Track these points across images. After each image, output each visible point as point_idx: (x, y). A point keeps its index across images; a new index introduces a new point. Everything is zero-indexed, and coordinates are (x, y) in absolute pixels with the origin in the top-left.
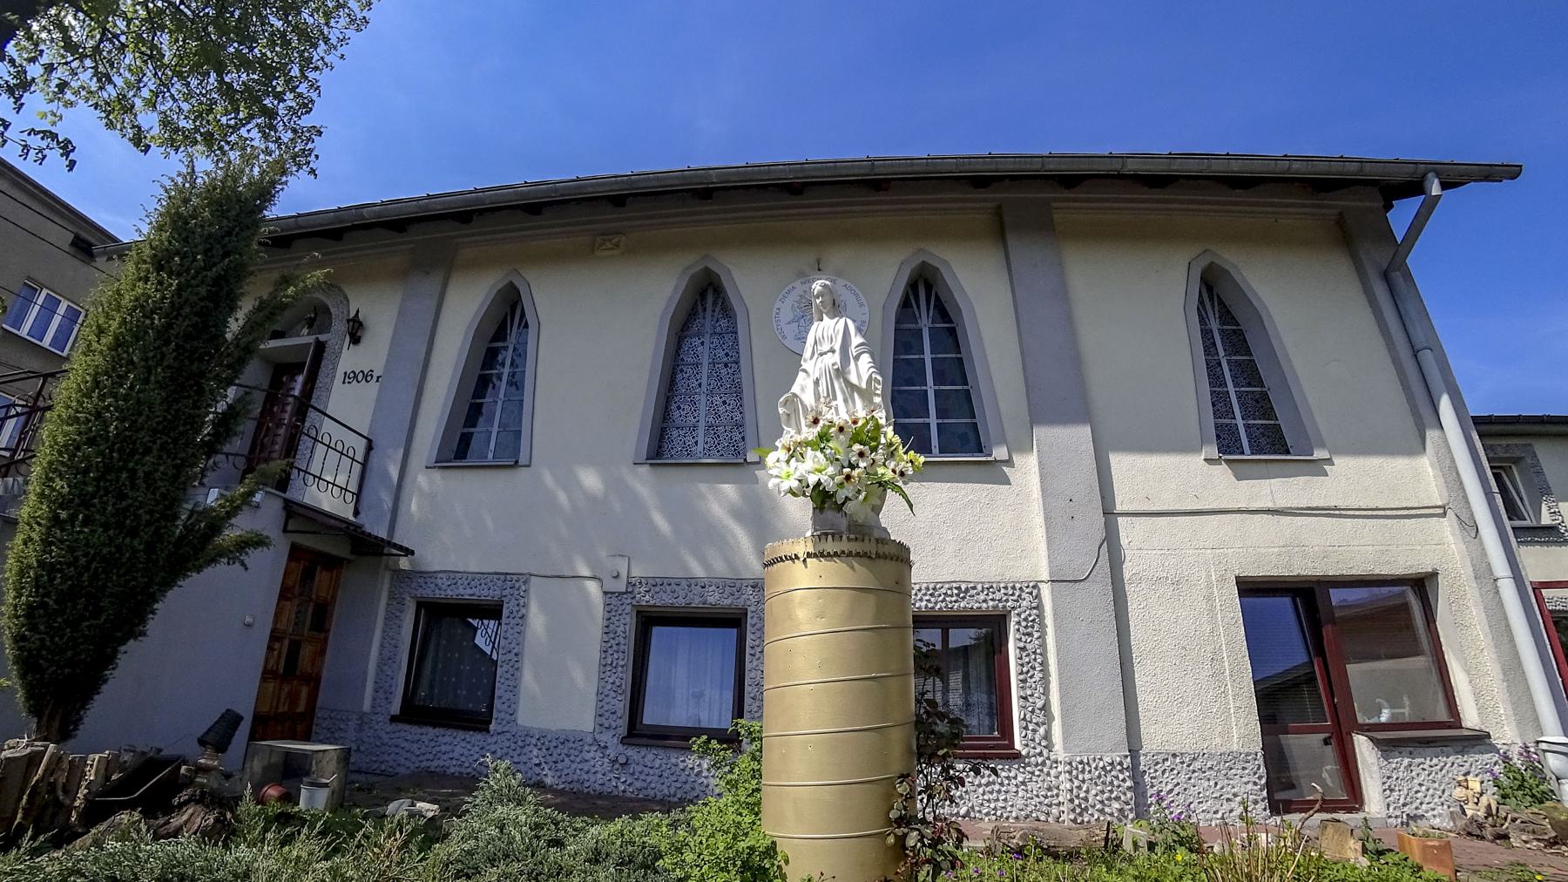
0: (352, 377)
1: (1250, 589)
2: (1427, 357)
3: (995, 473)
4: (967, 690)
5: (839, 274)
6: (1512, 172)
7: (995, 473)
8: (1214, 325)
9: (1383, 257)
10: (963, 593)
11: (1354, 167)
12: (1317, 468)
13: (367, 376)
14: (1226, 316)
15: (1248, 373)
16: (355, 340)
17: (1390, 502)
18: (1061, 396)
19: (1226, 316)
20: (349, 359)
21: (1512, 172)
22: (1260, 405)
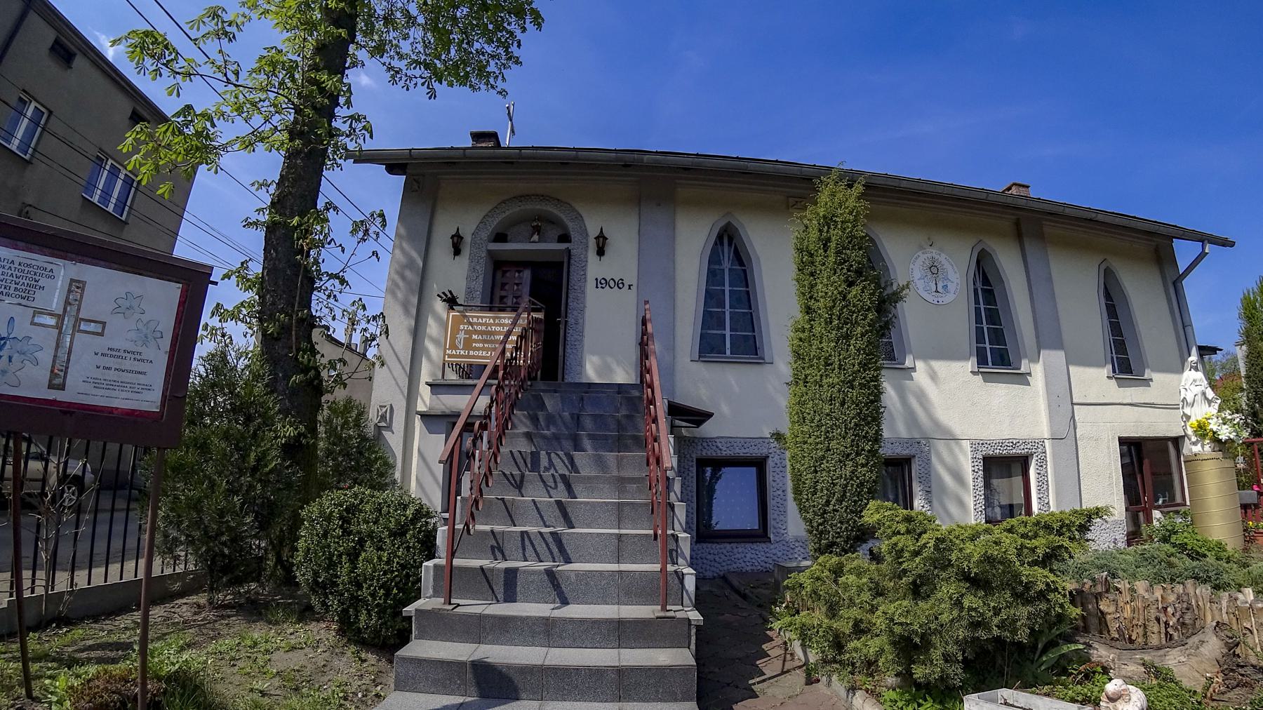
0: (602, 283)
1: (1122, 441)
2: (1188, 329)
3: (1023, 379)
4: (272, 460)
5: (941, 250)
6: (1232, 244)
7: (1023, 379)
8: (979, 286)
9: (1171, 277)
10: (1014, 445)
11: (984, 196)
12: (1147, 383)
13: (619, 284)
14: (986, 281)
15: (993, 317)
16: (601, 252)
17: (1185, 401)
18: (1050, 338)
19: (986, 281)
20: (595, 268)
21: (1232, 244)
22: (998, 337)
